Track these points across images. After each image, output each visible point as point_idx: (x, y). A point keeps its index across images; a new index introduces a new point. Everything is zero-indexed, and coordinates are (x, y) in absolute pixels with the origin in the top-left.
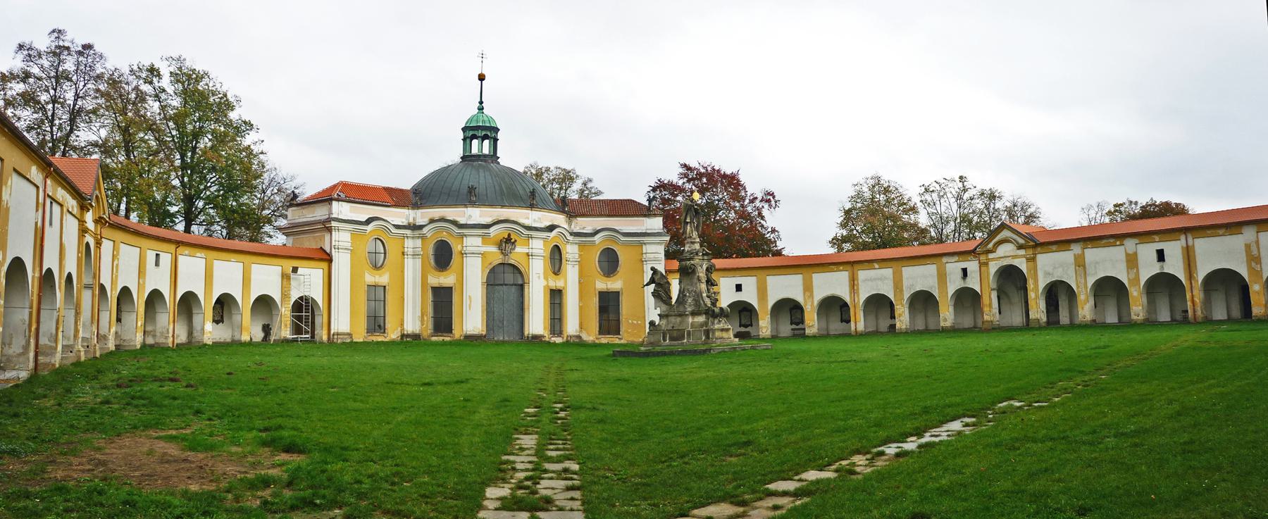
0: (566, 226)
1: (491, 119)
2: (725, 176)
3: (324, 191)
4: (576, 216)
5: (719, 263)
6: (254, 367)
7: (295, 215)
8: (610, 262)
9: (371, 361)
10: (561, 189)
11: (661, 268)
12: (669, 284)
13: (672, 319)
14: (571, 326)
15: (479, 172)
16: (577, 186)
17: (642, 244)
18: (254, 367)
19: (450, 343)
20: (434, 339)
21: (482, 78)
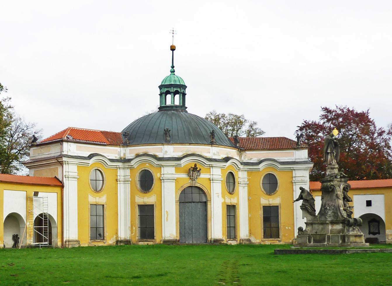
0: (238, 158)
1: (180, 79)
2: (357, 115)
3: (56, 135)
4: (245, 150)
5: (353, 184)
6: (7, 266)
7: (35, 153)
8: (271, 184)
9: (94, 260)
10: (233, 130)
11: (307, 188)
12: (314, 200)
13: (316, 226)
14: (243, 233)
15: (171, 120)
16: (245, 128)
17: (292, 170)
18: (7, 266)
19: (153, 247)
20: (141, 243)
21: (173, 49)
